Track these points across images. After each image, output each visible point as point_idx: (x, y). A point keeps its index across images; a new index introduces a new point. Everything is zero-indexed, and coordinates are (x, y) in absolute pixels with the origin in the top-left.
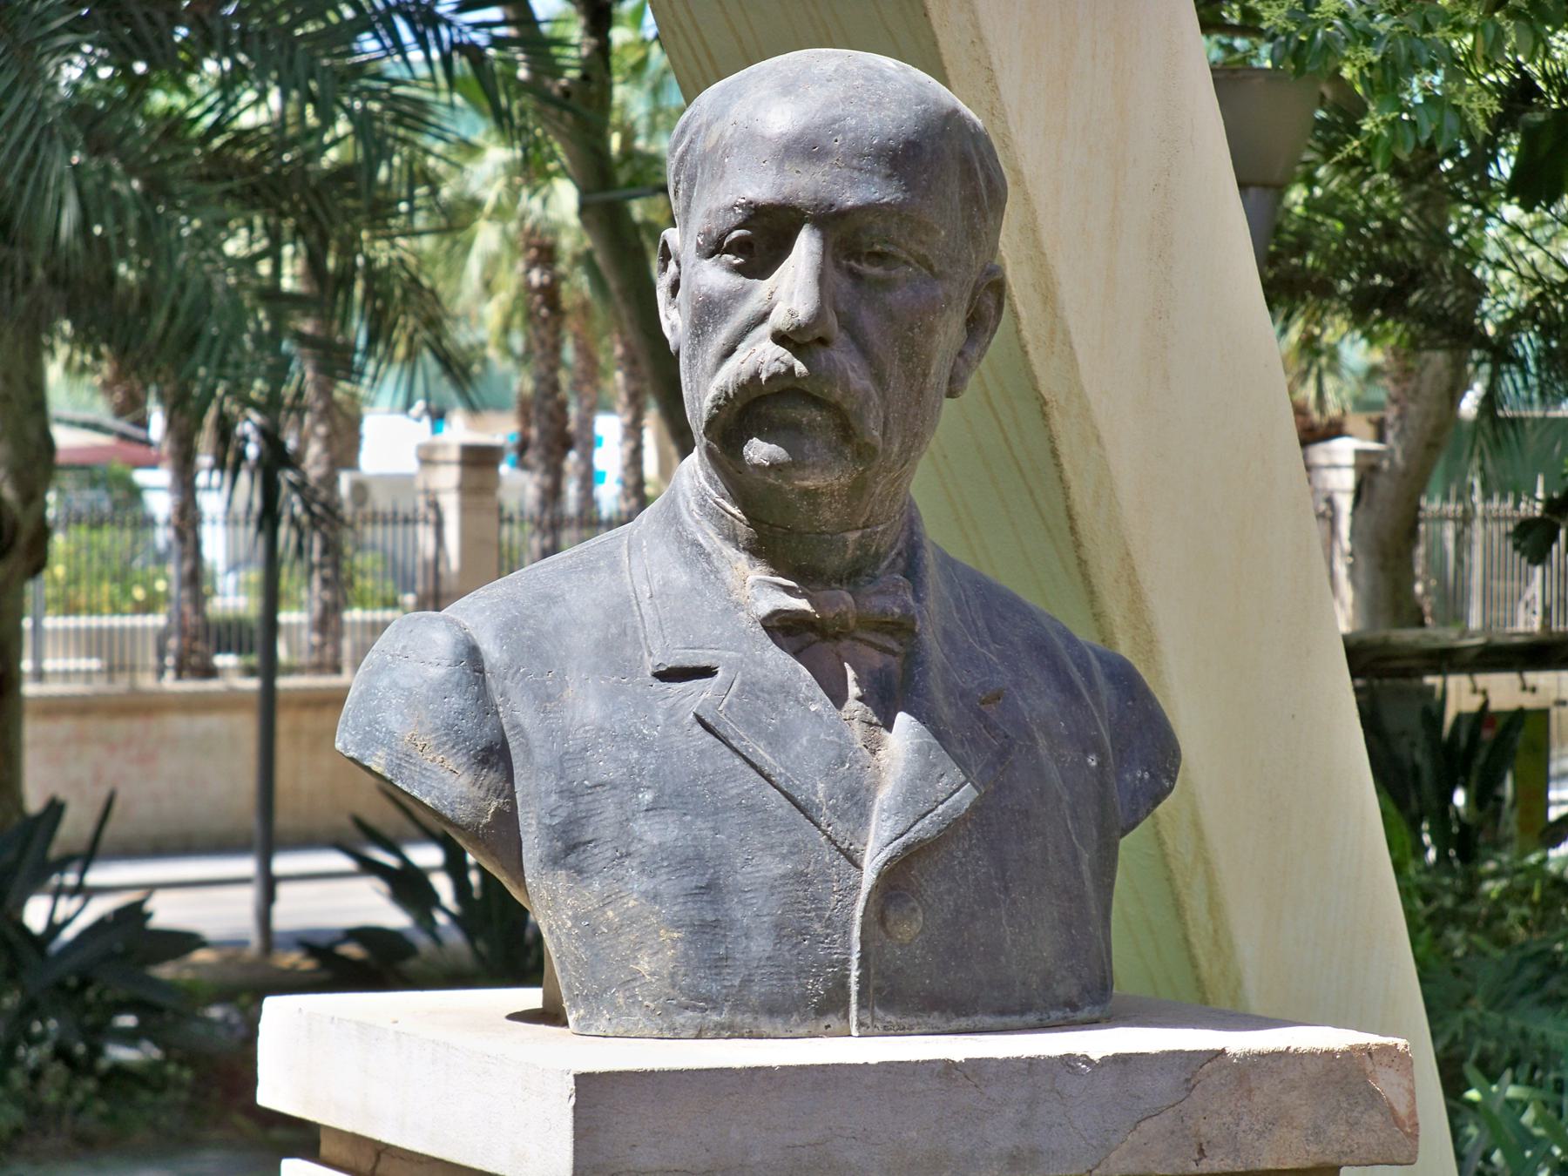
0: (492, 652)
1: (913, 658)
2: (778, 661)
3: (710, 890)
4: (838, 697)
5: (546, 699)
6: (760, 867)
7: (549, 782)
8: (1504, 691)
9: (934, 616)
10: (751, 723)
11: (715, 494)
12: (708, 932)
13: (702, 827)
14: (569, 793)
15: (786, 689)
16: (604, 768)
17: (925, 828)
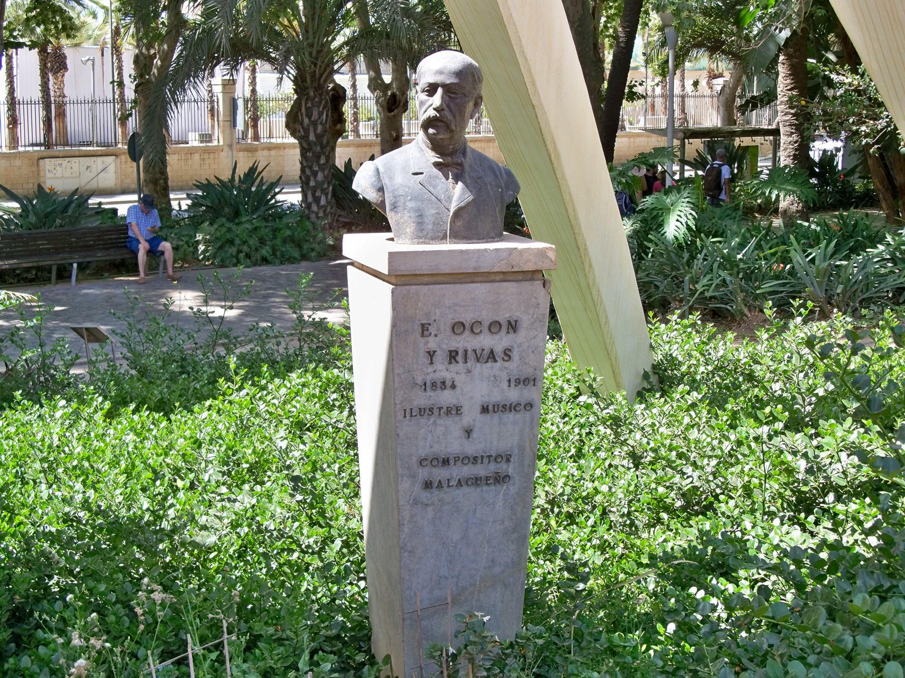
0: (381, 170)
1: (463, 171)
2: (436, 171)
3: (421, 216)
4: (447, 179)
5: (391, 179)
6: (430, 212)
7: (391, 195)
8: (747, 141)
9: (467, 162)
10: (430, 184)
11: (425, 138)
12: (420, 224)
13: (420, 204)
14: (395, 197)
15: (437, 177)
16: (401, 192)
17: (462, 204)
